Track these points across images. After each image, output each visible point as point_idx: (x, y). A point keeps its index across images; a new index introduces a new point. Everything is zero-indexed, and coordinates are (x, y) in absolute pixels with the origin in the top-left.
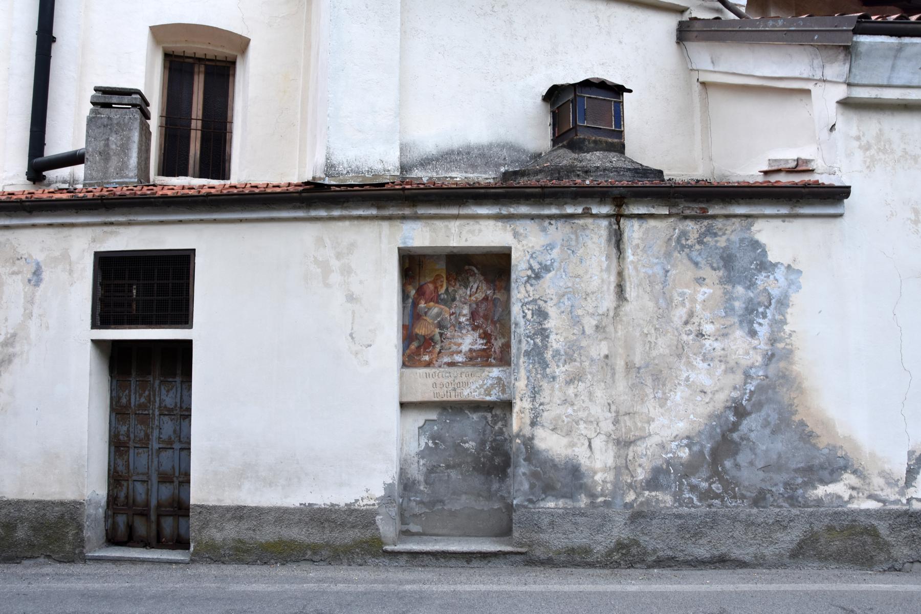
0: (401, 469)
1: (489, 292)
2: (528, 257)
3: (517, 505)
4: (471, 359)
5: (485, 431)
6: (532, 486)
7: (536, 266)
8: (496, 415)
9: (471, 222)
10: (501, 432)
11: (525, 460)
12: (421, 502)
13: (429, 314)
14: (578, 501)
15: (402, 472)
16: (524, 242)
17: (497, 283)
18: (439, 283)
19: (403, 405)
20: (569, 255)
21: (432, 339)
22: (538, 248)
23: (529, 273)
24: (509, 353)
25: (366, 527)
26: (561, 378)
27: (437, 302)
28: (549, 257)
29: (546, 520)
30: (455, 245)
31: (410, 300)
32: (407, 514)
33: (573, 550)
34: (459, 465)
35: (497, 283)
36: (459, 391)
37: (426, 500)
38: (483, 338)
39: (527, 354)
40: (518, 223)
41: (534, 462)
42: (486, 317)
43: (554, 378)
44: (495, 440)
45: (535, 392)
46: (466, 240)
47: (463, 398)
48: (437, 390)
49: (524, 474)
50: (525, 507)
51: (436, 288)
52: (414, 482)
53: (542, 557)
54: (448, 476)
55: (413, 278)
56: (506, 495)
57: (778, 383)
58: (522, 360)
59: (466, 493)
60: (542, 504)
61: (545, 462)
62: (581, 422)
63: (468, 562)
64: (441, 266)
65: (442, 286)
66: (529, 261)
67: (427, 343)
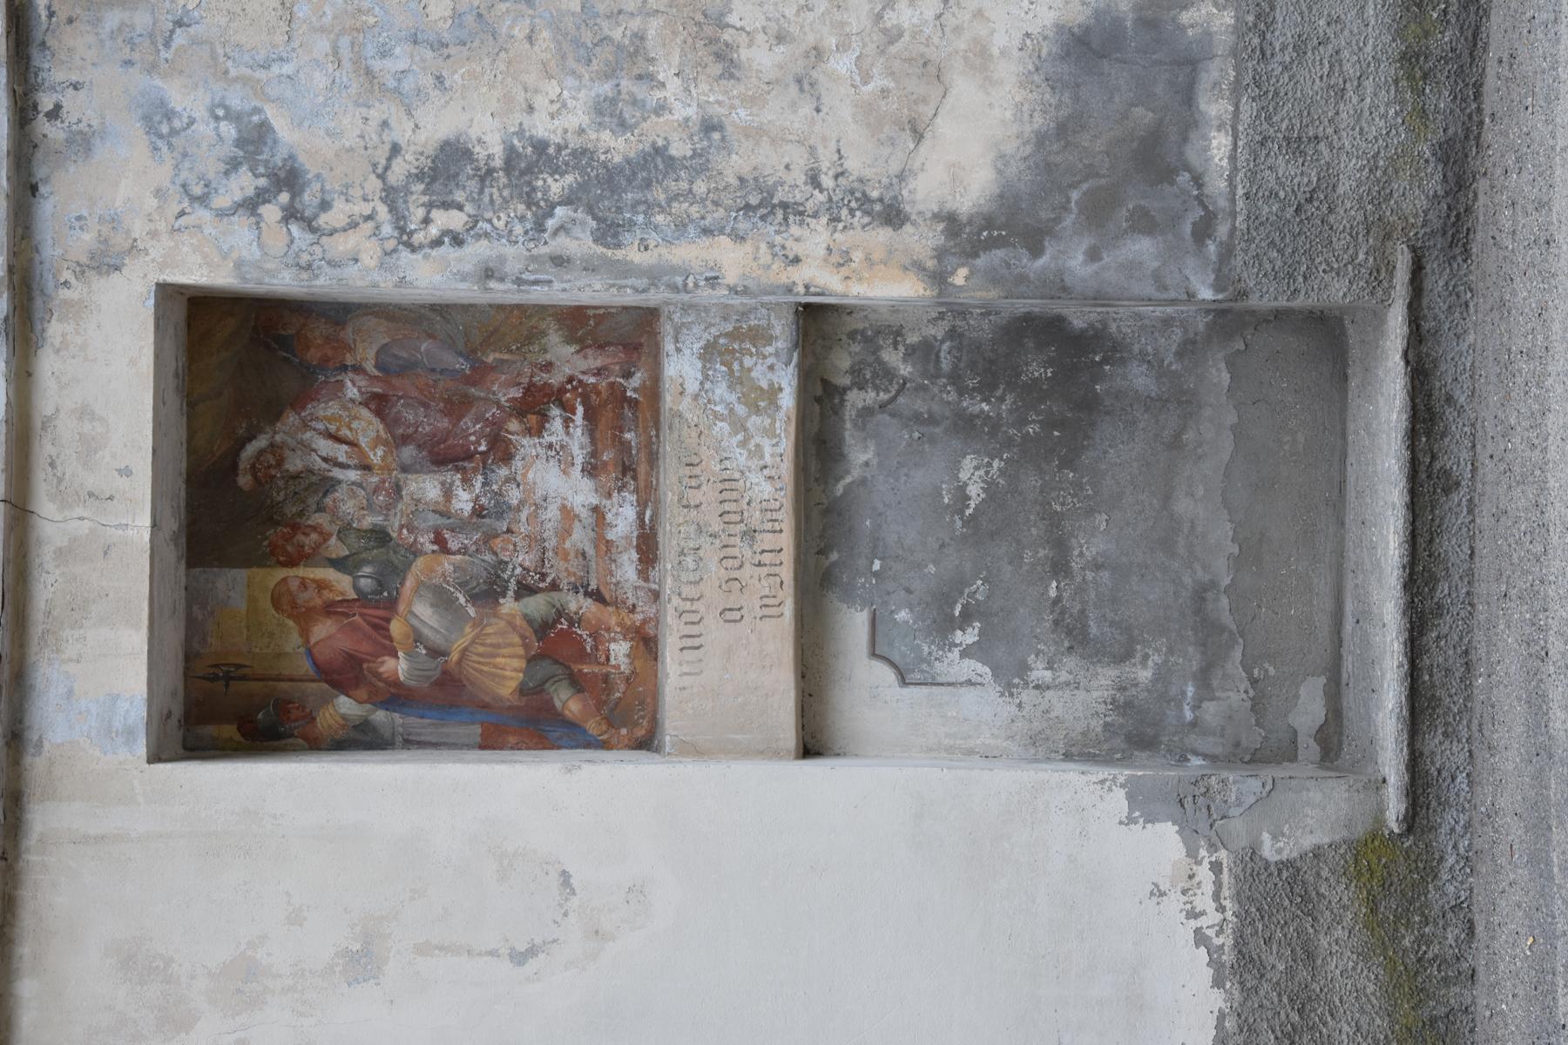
0: (1068, 757)
1: (352, 392)
2: (202, 215)
3: (1218, 287)
4: (627, 469)
5: (917, 418)
6: (1144, 223)
7: (244, 183)
8: (855, 371)
9: (44, 449)
10: (924, 352)
11: (1036, 251)
12: (1204, 678)
13: (437, 640)
14: (1208, 34)
15: (1080, 752)
16: (138, 228)
17: (313, 356)
18: (311, 598)
19: (810, 748)
20: (195, 41)
21: (542, 628)
22: (162, 174)
23: (271, 212)
24: (604, 315)
25: (1307, 903)
26: (711, 96)
27: (392, 604)
28: (204, 129)
29: (1284, 169)
30: (146, 521)
31: (380, 716)
32: (1253, 738)
33: (1409, 59)
34: (1054, 521)
35: (313, 356)
36: (755, 518)
37: (1193, 659)
38: (544, 418)
39: (609, 232)
40: (50, 251)
41: (1045, 215)
42: (457, 407)
43: (709, 126)
44: (955, 378)
45: (766, 205)
46: (126, 472)
47: (786, 499)
48: (752, 603)
49: (1093, 255)
50: (1227, 252)
51: (330, 609)
52: (1124, 707)
53: (1434, 184)
54: (1097, 567)
55: (283, 706)
56: (1177, 335)
57: (736, 366)
58: (635, 256)
59: (1167, 498)
60: (1217, 185)
61: (1049, 168)
62: (891, 19)
63: (1450, 484)
64: (236, 586)
65: (321, 585)
66: (221, 214)
67: (555, 645)
